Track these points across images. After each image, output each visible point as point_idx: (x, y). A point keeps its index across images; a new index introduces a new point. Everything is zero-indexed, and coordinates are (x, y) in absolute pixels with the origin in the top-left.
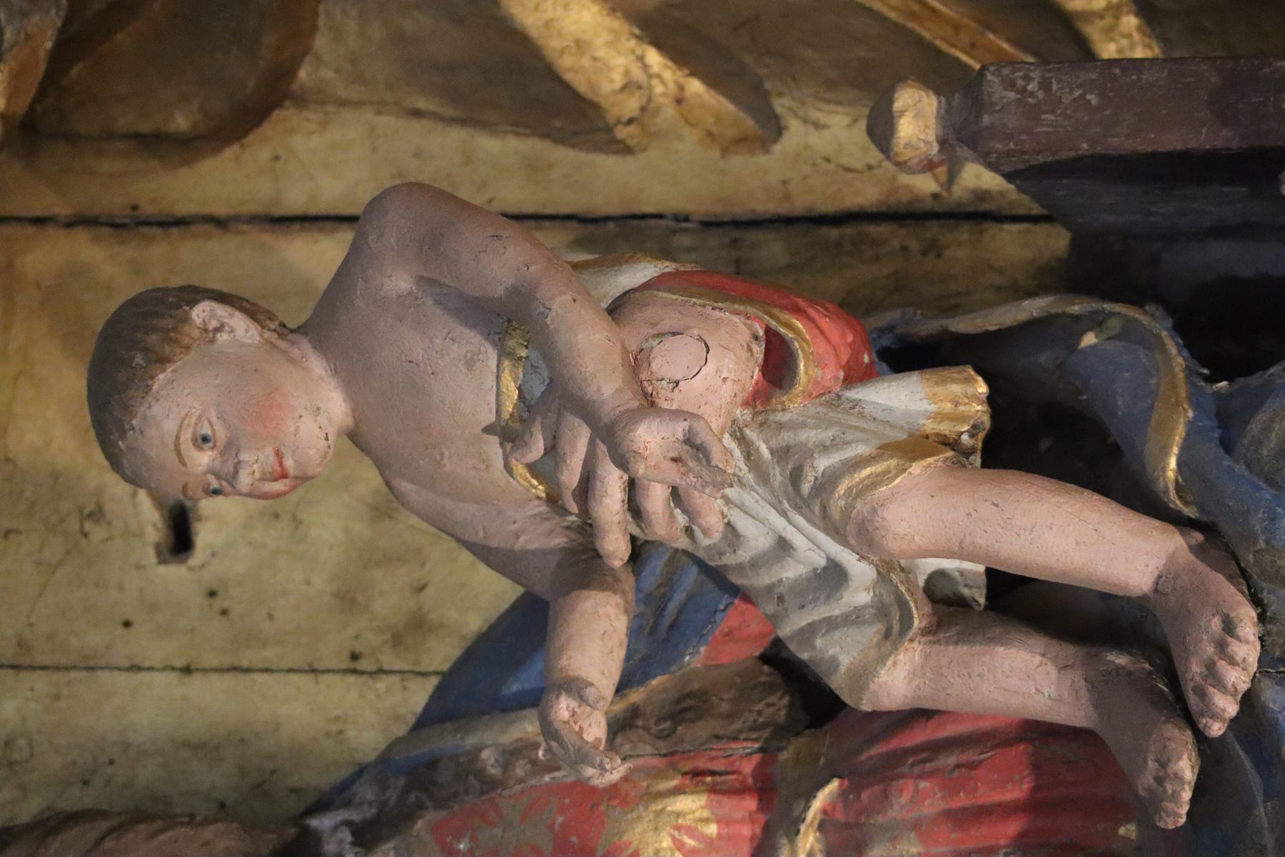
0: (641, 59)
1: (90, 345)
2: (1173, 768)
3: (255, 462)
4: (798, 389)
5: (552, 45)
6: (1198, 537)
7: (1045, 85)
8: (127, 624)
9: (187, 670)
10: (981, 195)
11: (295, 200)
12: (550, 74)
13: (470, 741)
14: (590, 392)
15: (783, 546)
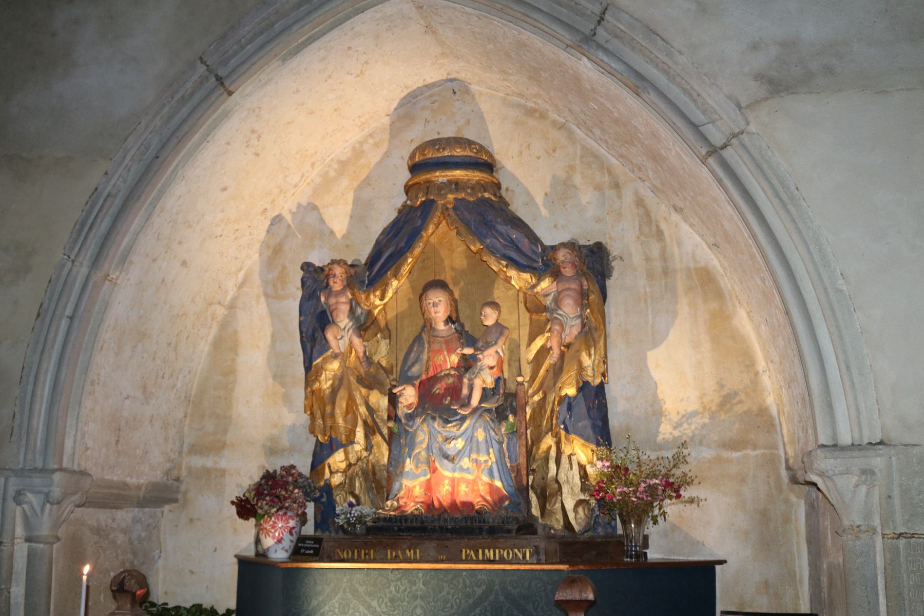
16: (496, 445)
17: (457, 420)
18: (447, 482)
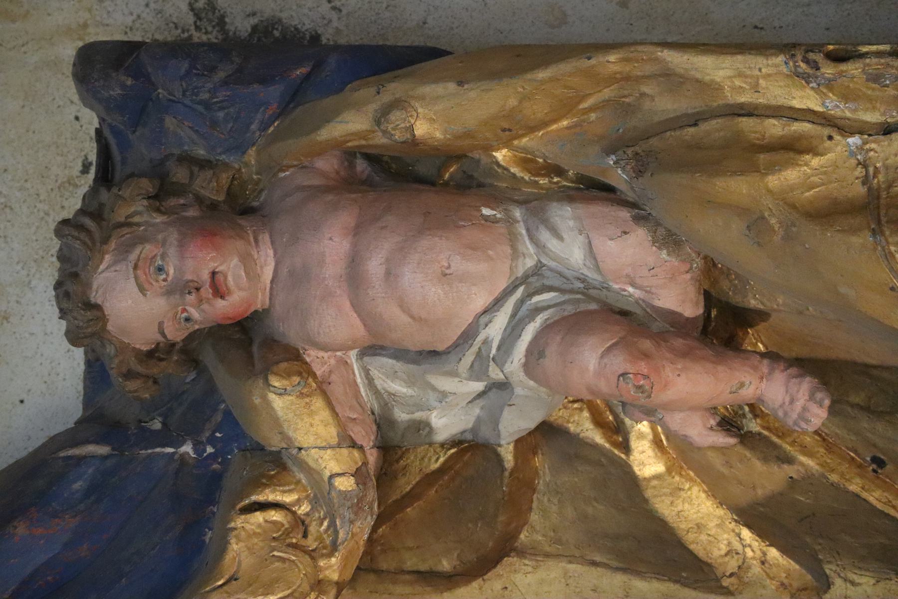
0: (739, 535)
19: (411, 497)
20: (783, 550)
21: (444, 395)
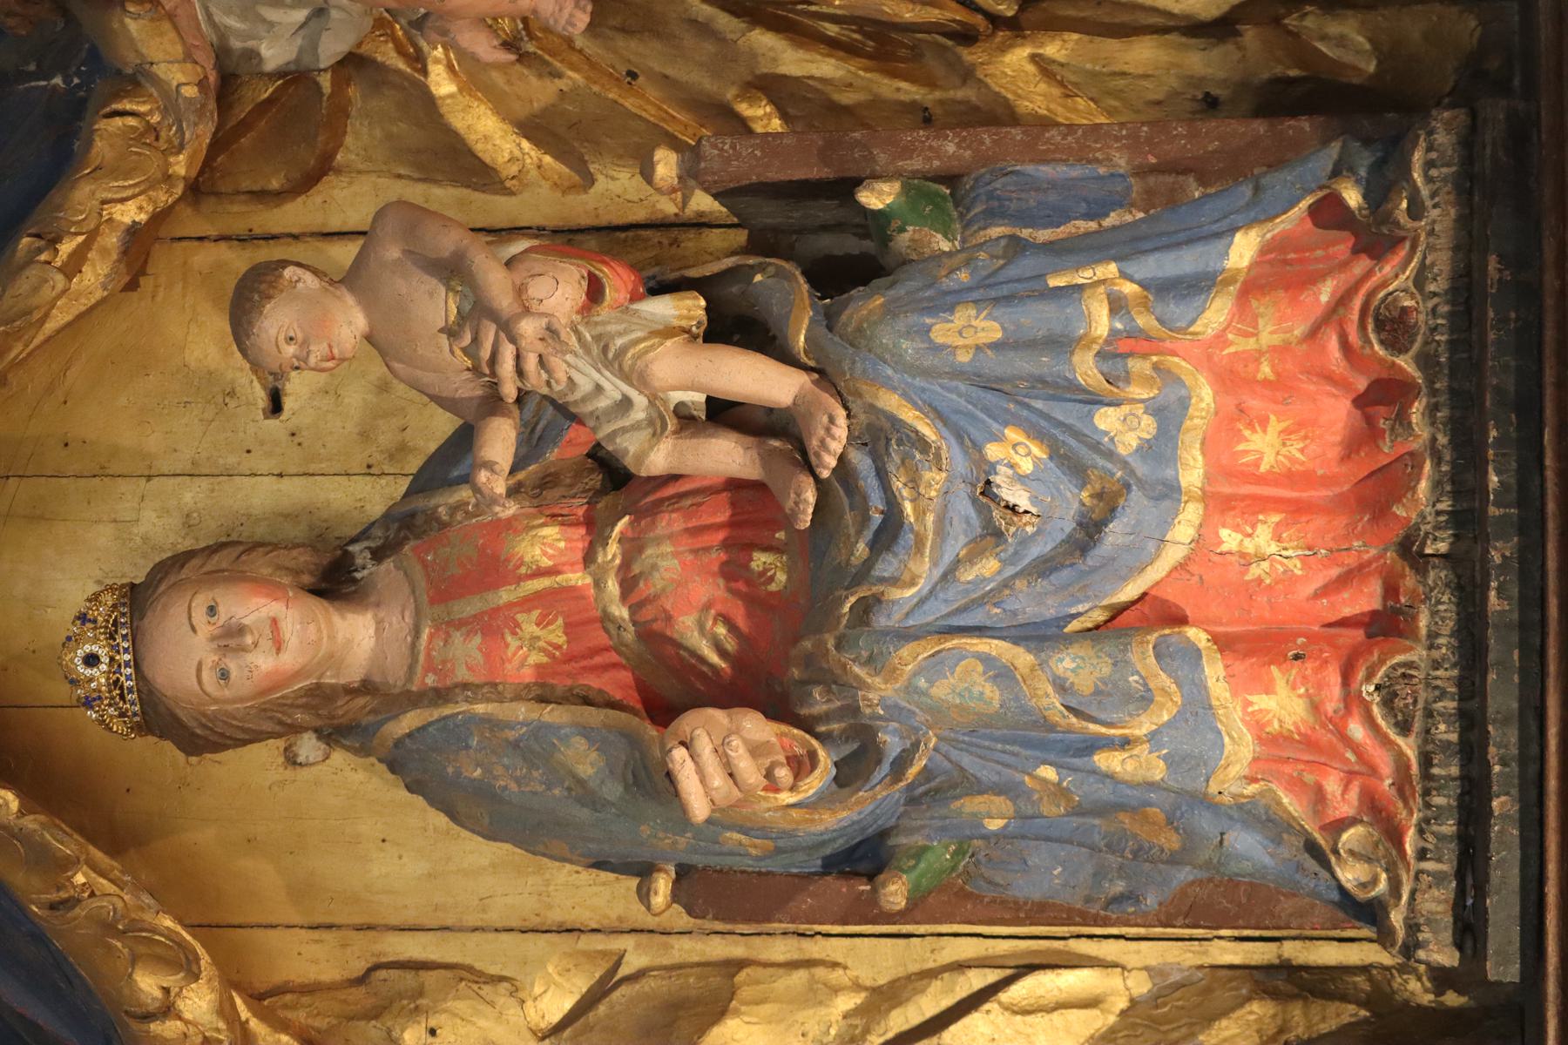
0: (519, 145)
1: (227, 304)
2: (803, 497)
3: (318, 351)
4: (606, 304)
5: (471, 138)
6: (816, 376)
7: (733, 147)
8: (249, 452)
9: (281, 475)
10: (701, 214)
11: (335, 224)
12: (471, 153)
13: (433, 502)
14: (495, 305)
15: (599, 389)
16: (1026, 265)
17: (882, 475)
18: (1230, 539)
19: (245, 125)
20: (556, 157)
21: (271, 24)
